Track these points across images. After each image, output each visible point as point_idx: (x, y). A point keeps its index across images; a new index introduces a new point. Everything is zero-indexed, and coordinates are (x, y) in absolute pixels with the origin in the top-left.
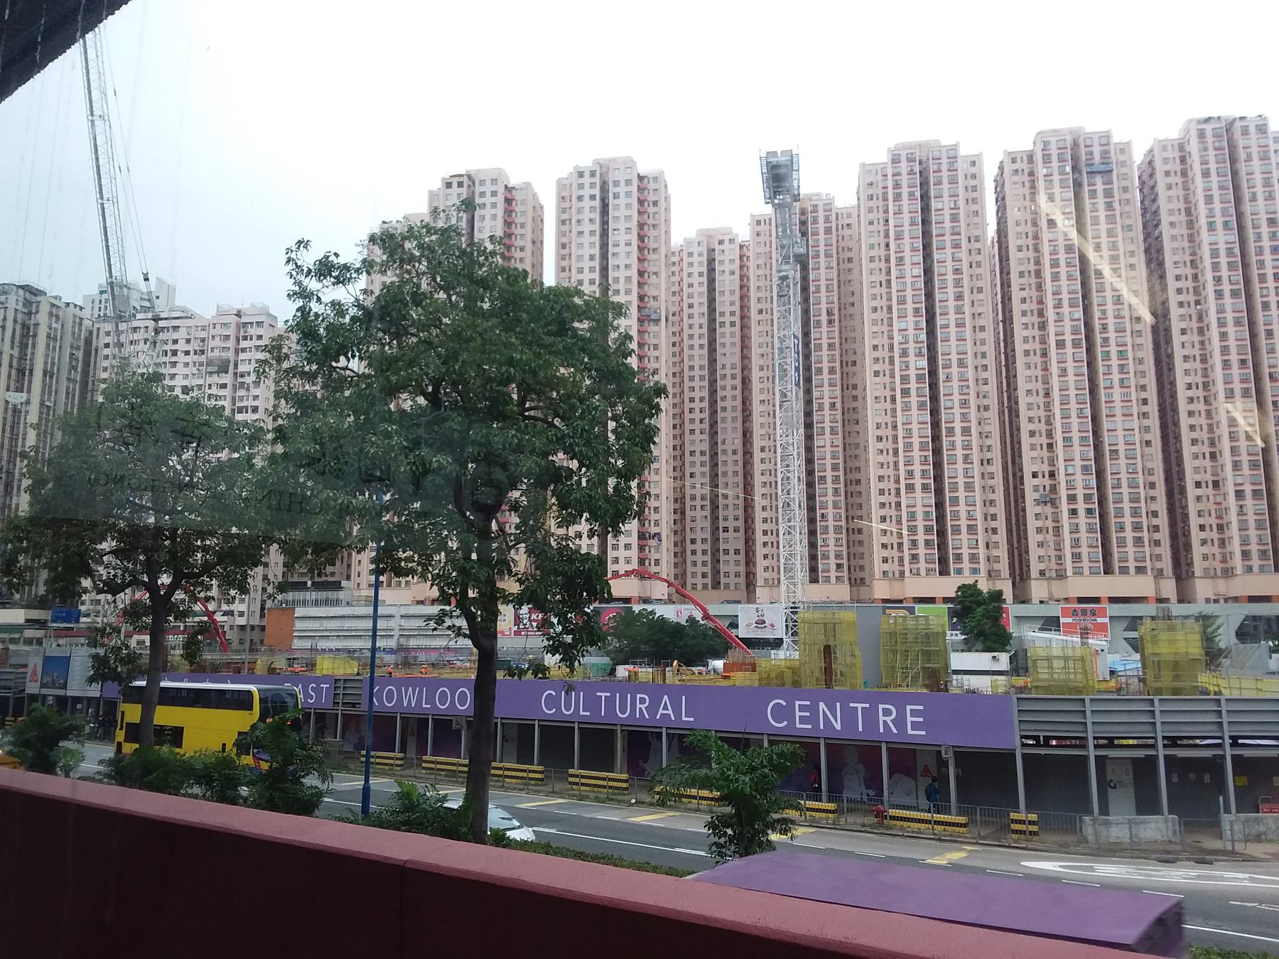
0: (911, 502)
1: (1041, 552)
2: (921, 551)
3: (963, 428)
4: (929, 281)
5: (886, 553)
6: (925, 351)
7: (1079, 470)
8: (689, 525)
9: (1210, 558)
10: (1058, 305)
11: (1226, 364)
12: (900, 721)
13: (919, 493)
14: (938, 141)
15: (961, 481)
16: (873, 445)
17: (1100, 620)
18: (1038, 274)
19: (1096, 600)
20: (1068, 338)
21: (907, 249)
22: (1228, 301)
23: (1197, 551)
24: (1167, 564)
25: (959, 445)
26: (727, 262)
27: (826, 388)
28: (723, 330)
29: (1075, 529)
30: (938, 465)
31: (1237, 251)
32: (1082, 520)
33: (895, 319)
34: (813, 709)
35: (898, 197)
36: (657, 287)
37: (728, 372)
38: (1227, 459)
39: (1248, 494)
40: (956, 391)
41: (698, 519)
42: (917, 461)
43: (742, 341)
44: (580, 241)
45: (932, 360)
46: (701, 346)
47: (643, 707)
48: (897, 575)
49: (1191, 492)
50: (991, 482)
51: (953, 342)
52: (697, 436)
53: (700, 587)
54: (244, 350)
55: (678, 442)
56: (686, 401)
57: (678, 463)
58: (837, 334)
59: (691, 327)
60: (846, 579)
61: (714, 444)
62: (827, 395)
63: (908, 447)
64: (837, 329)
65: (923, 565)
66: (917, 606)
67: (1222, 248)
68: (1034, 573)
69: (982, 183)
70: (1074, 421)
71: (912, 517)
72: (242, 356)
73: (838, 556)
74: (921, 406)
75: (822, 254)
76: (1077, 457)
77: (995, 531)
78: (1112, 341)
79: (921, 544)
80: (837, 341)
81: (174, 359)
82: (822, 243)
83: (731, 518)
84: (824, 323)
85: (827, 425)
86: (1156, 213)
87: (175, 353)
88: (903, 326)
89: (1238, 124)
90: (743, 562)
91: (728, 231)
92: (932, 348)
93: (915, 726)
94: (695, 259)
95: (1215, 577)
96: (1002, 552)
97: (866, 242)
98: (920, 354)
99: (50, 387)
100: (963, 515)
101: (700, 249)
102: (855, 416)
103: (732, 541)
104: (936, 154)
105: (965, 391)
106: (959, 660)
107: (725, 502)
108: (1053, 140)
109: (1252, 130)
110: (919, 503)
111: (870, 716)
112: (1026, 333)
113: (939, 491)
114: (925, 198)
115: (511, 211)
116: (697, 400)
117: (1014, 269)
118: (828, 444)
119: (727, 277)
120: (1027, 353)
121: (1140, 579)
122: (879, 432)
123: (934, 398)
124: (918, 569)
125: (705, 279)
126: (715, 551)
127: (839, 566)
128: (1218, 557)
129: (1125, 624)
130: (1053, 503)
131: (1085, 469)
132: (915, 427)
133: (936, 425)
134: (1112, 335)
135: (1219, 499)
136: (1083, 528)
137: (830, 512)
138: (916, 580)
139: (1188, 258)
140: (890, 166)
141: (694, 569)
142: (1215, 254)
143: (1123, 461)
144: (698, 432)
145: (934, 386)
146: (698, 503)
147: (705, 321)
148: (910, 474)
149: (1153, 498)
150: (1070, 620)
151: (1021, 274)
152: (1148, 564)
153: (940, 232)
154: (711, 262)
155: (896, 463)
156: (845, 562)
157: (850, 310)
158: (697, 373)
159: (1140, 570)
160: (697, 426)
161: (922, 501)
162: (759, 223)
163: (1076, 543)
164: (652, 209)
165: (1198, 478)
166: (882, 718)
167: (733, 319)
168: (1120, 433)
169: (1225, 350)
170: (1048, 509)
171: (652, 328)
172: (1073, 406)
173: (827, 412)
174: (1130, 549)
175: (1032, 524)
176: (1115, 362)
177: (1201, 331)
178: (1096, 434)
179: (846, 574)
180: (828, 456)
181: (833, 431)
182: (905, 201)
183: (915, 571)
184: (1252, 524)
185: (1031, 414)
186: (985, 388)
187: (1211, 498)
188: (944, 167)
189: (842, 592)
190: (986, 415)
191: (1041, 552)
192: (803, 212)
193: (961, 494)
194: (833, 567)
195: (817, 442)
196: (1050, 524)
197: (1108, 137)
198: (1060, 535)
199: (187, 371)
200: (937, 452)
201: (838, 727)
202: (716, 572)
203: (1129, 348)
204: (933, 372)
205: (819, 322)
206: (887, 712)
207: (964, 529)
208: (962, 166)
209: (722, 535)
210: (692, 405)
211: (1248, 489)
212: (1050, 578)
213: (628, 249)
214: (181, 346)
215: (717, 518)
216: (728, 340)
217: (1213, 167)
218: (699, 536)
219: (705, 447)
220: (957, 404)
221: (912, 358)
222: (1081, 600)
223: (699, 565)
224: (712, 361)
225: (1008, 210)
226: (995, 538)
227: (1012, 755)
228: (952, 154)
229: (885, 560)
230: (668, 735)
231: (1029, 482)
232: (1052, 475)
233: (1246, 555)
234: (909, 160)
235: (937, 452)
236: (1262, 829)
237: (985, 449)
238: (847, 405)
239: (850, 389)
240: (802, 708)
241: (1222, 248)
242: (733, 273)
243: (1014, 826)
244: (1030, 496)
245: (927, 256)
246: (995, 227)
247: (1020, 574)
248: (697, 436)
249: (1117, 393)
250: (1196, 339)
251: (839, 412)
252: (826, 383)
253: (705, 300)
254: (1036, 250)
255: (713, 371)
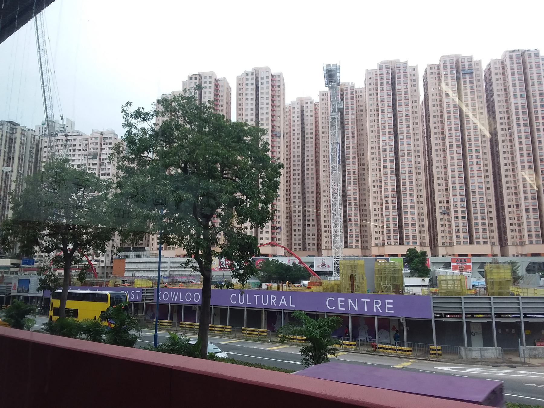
0: (388, 214)
1: (443, 235)
2: (392, 234)
3: (410, 182)
4: (395, 120)
5: (377, 235)
6: (393, 149)
7: (459, 200)
8: (293, 223)
9: (515, 237)
10: (450, 130)
11: (522, 155)
12: (383, 307)
13: (391, 210)
14: (399, 60)
15: (409, 205)
16: (371, 189)
17: (468, 264)
18: (442, 117)
19: (466, 255)
20: (454, 144)
21: (386, 106)
22: (522, 128)
23: (509, 234)
24: (496, 240)
25: (408, 189)
26: (309, 111)
27: (351, 165)
28: (307, 140)
29: (457, 225)
30: (399, 198)
31: (526, 107)
32: (460, 221)
33: (381, 136)
34: (346, 302)
35: (382, 84)
36: (280, 122)
37: (310, 158)
38: (522, 195)
39: (531, 210)
40: (407, 166)
41: (297, 221)
42: (390, 196)
43: (316, 145)
44: (247, 102)
45: (397, 153)
46: (298, 147)
47: (274, 301)
48: (382, 245)
49: (507, 209)
50: (421, 205)
51: (405, 146)
52: (297, 186)
53: (298, 250)
54: (104, 149)
55: (288, 188)
56: (292, 170)
57: (288, 197)
58: (356, 142)
59: (294, 139)
60: (360, 246)
61: (304, 189)
62: (352, 168)
63: (386, 190)
64: (356, 140)
65: (392, 241)
66: (390, 258)
67: (520, 106)
68: (440, 244)
69: (418, 78)
70: (457, 179)
71: (388, 220)
72: (103, 151)
73: (356, 237)
74: (392, 173)
75: (350, 108)
76: (458, 194)
77: (423, 226)
78: (473, 145)
79: (392, 231)
80: (356, 145)
81: (74, 153)
82: (350, 103)
83: (311, 220)
84: (351, 137)
85: (352, 181)
86: (492, 90)
87: (74, 150)
88: (384, 139)
89: (527, 53)
90: (316, 239)
91: (310, 98)
92: (396, 148)
93: (389, 309)
94: (296, 110)
95: (517, 245)
96: (426, 235)
97: (368, 103)
98: (391, 151)
99: (21, 165)
100: (410, 219)
101: (298, 106)
102: (364, 177)
103: (311, 230)
104: (398, 66)
105: (411, 166)
106: (408, 281)
107: (308, 213)
108: (448, 60)
109: (533, 55)
110: (391, 214)
111: (370, 305)
112: (436, 142)
113: (399, 209)
114: (393, 84)
115: (217, 90)
116: (297, 170)
117: (431, 114)
118: (352, 189)
119: (309, 118)
120: (437, 150)
121: (485, 246)
122: (374, 184)
123: (397, 169)
124: (391, 242)
125: (300, 119)
126: (304, 235)
127: (357, 241)
128: (518, 237)
129: (478, 266)
130: (448, 214)
131: (462, 200)
132: (389, 182)
133: (398, 181)
134: (473, 142)
135: (519, 212)
136: (461, 225)
137: (353, 218)
138: (390, 247)
139: (505, 110)
140: (378, 71)
141: (295, 242)
142: (517, 108)
143: (477, 196)
144: (297, 184)
145: (397, 164)
146: (297, 214)
147: (300, 136)
148: (387, 202)
149: (490, 212)
150: (455, 264)
151: (434, 117)
152: (488, 240)
153: (400, 99)
154: (302, 111)
155: (381, 197)
156: (359, 239)
157: (362, 132)
158: (296, 158)
159: (485, 243)
160: (296, 181)
161: (392, 213)
162: (323, 95)
163: (458, 231)
164: (277, 89)
165: (510, 203)
166: (375, 306)
167: (312, 136)
168: (476, 184)
169: (521, 149)
170: (446, 217)
171: (277, 140)
172: (457, 173)
173: (352, 175)
174: (481, 234)
175: (439, 223)
176: (474, 154)
177: (511, 141)
178: (466, 184)
179: (360, 244)
180: (352, 194)
181: (354, 183)
182: (385, 86)
183: (389, 243)
184: (532, 223)
185: (438, 176)
186: (419, 165)
187: (515, 212)
188: (402, 71)
189: (358, 252)
190: (419, 176)
191: (443, 235)
192: (342, 90)
193: (409, 210)
194: (354, 241)
195: (348, 188)
196: (446, 223)
197: (471, 58)
198: (451, 227)
199: (79, 158)
200: (399, 192)
201: (356, 309)
202: (305, 243)
203: (480, 148)
204: (397, 158)
205: (348, 137)
206: (377, 303)
207: (410, 225)
208: (409, 71)
209: (307, 228)
210: (294, 172)
211: (531, 208)
212: (447, 246)
213: (267, 106)
214: (77, 147)
215: (305, 220)
216: (310, 145)
217: (516, 71)
218: (297, 228)
219: (300, 190)
220: (407, 172)
221: (388, 152)
222: (460, 255)
223: (297, 240)
224: (303, 153)
225: (429, 89)
226: (423, 229)
227: (430, 321)
228: (405, 65)
229: (376, 238)
230: (284, 313)
231: (438, 205)
232: (447, 202)
233: (530, 236)
234: (387, 68)
235: (399, 192)
236: (537, 353)
237: (419, 191)
238: (360, 172)
239: (362, 166)
240: (341, 301)
241: (520, 106)
242: (312, 116)
243: (431, 352)
244: (438, 211)
245: (394, 109)
246: (423, 97)
247: (434, 244)
248: (297, 186)
249: (475, 167)
250: (509, 144)
251: (357, 175)
252: (351, 163)
253: (300, 128)
254: (441, 106)
255: (303, 158)
